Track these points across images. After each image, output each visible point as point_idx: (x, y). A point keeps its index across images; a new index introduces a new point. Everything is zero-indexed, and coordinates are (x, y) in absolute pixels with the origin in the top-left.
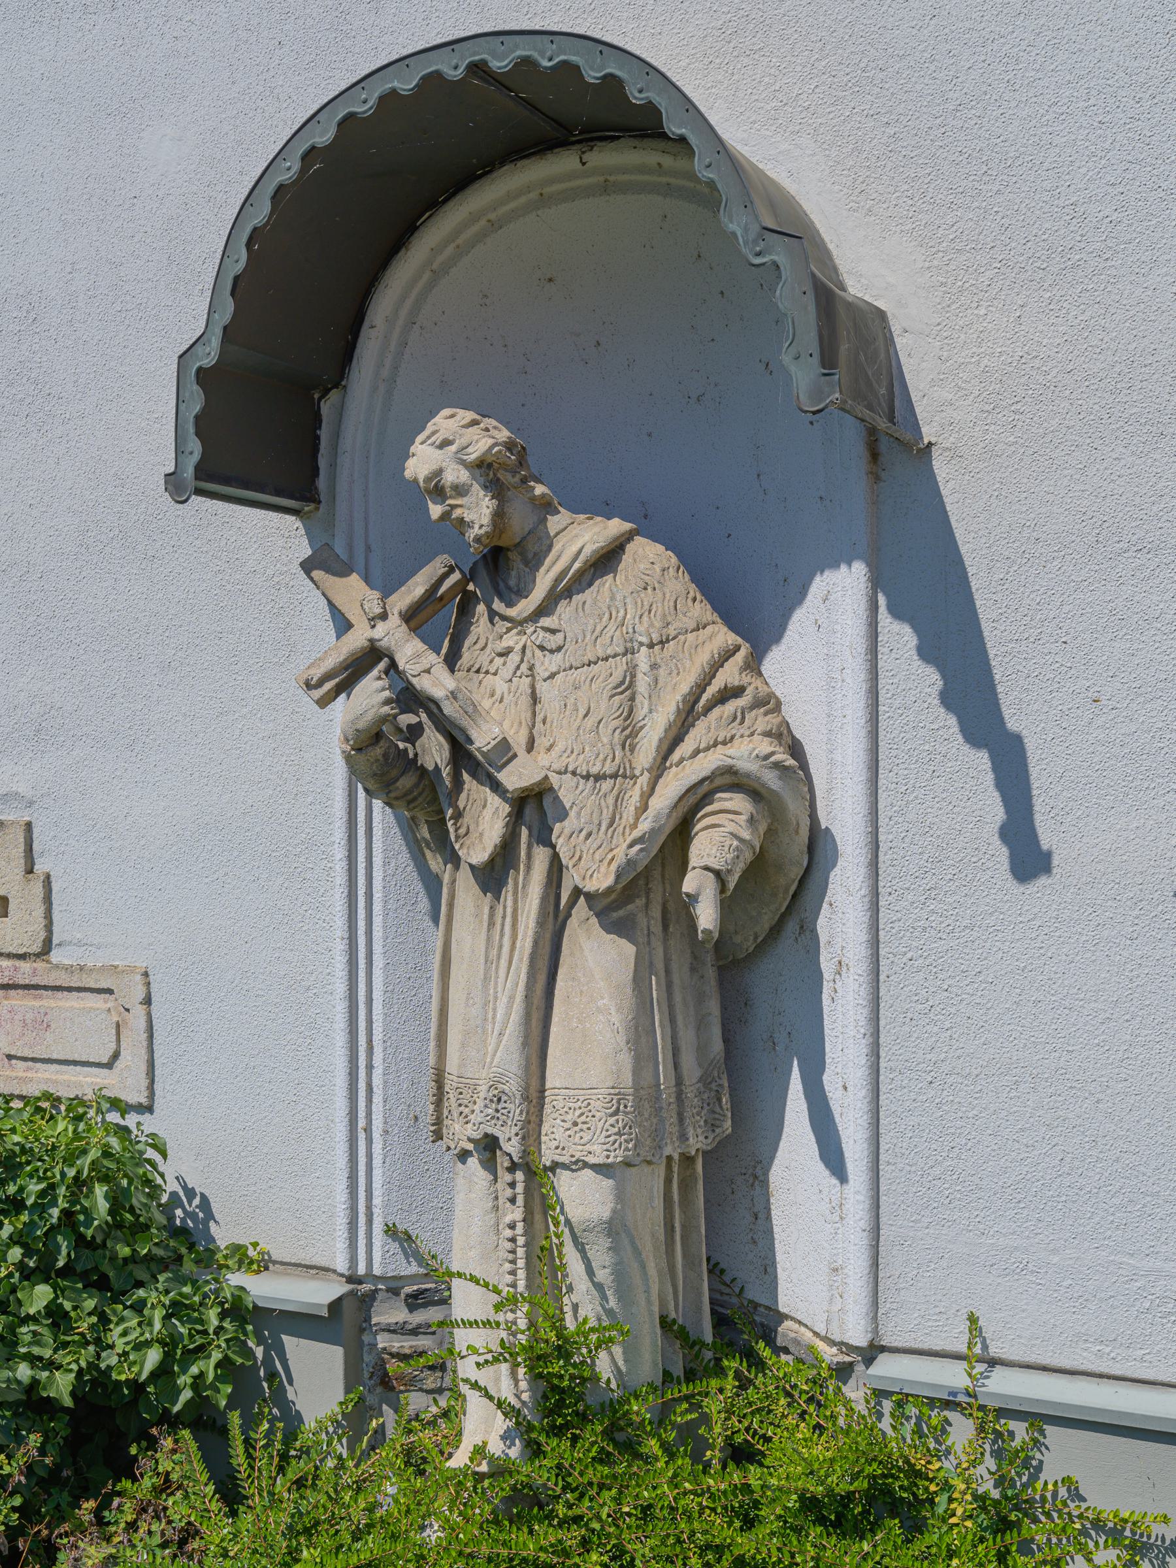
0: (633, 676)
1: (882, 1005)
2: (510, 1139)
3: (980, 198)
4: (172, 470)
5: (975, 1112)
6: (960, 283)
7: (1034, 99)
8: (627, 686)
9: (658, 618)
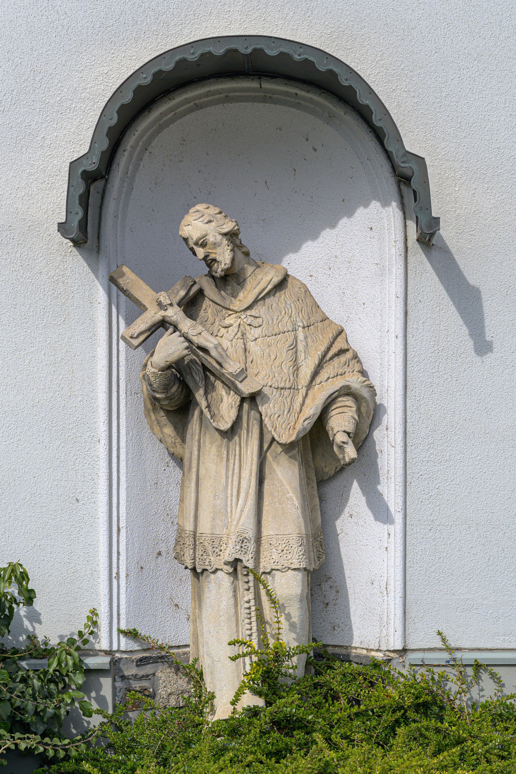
0: (296, 342)
1: (407, 496)
2: (248, 560)
3: (457, 138)
4: (64, 221)
5: (450, 541)
6: (447, 175)
7: (482, 99)
8: (294, 347)
9: (306, 314)
